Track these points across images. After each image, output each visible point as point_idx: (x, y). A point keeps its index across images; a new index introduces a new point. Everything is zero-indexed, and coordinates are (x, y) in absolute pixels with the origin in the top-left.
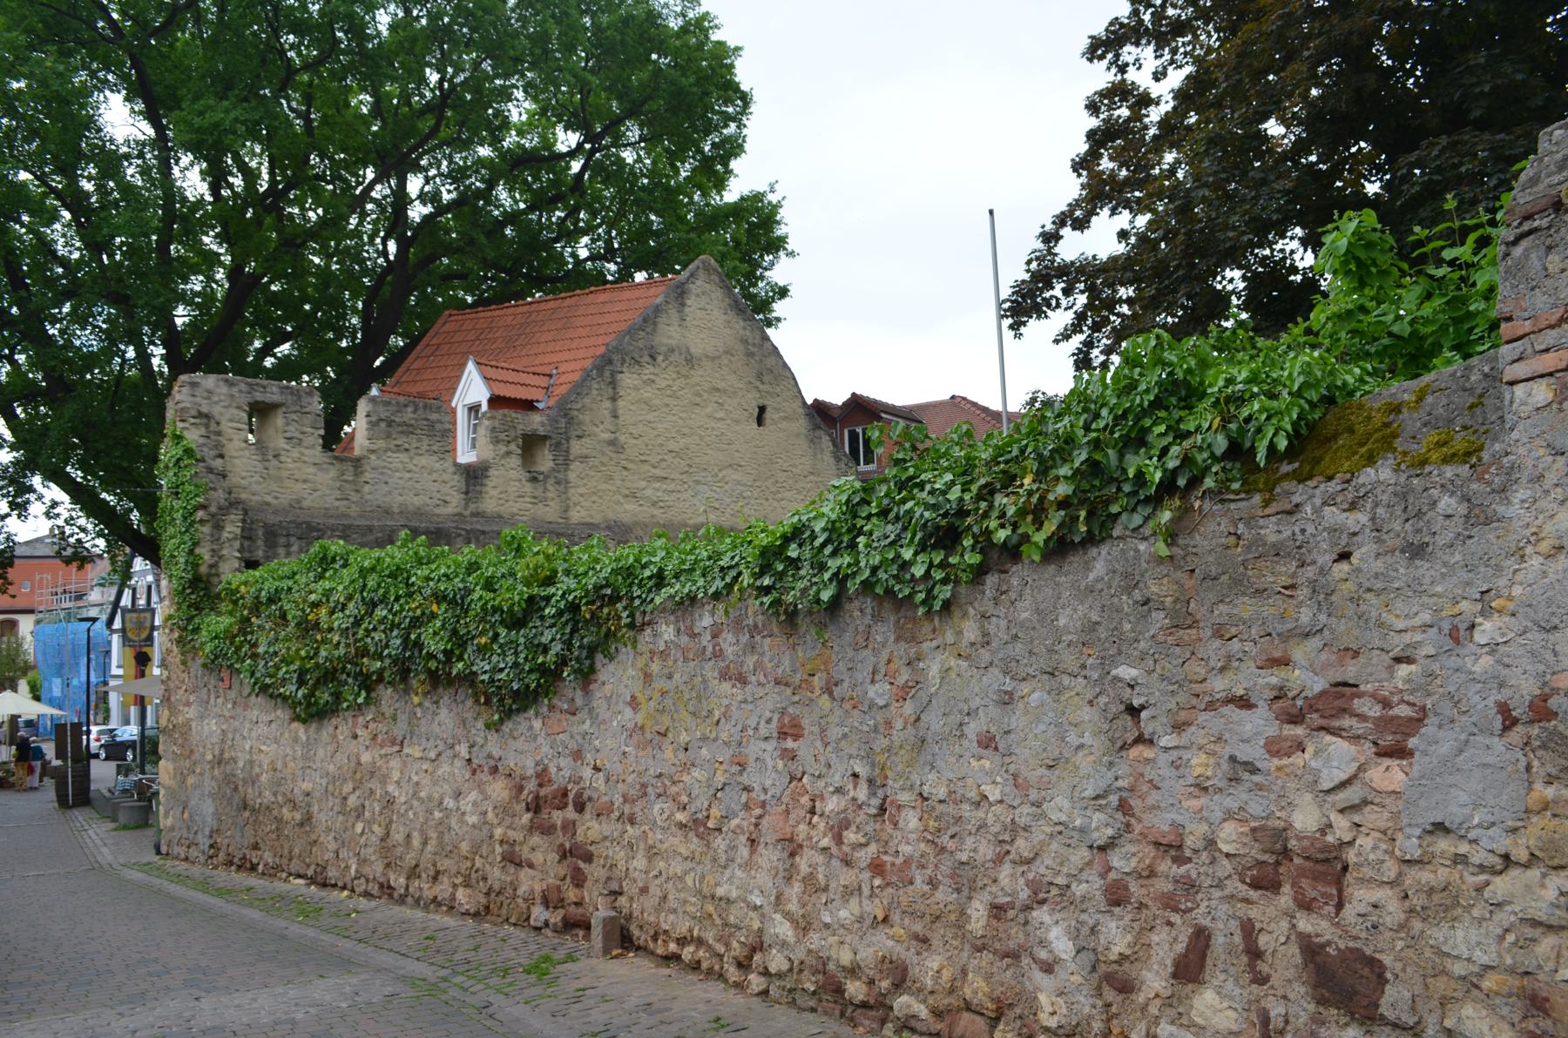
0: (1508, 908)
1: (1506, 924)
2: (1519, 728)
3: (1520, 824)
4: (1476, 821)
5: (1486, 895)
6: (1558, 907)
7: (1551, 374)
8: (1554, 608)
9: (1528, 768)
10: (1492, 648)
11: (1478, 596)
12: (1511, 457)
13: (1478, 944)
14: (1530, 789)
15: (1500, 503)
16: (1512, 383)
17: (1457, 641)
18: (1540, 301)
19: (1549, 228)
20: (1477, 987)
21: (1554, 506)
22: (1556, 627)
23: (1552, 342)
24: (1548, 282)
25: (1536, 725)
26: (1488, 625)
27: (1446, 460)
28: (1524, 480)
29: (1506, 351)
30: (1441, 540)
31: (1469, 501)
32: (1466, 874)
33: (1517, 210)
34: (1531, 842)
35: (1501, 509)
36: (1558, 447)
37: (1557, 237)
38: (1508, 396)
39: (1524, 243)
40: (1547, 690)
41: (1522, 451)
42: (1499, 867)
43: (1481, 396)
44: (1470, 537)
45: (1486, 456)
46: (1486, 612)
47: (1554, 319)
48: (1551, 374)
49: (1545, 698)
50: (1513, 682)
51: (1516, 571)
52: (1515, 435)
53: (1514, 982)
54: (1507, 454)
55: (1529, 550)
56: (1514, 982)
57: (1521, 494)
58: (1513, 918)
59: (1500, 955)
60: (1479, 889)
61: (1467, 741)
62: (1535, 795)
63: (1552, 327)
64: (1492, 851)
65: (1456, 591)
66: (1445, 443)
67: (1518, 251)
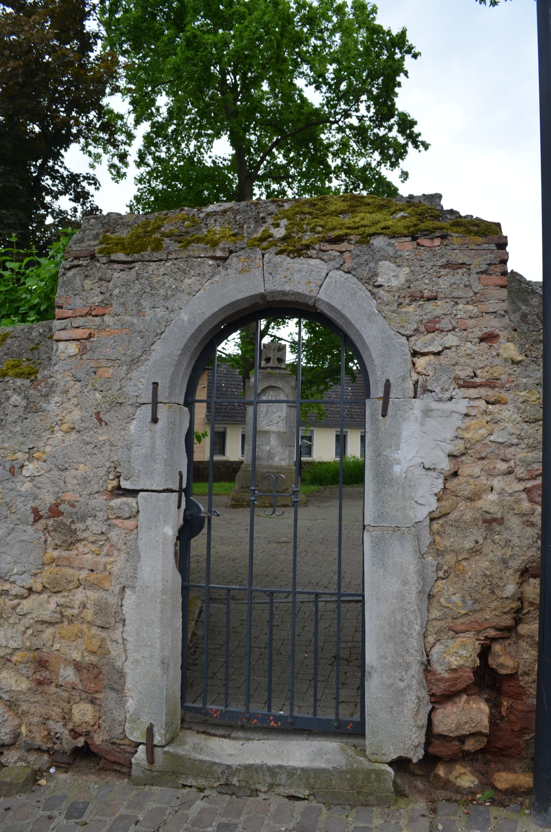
0: (29, 616)
1: (27, 625)
2: (42, 521)
3: (39, 571)
4: (15, 571)
5: (18, 611)
6: (55, 612)
7: (78, 340)
8: (66, 459)
9: (46, 541)
10: (32, 478)
11: (27, 450)
12: (53, 379)
13: (12, 637)
14: (45, 553)
15: (44, 402)
16: (58, 341)
17: (13, 474)
18: (78, 302)
19: (86, 266)
20: (9, 661)
21: (72, 407)
22: (66, 469)
23: (81, 324)
24: (84, 293)
25: (52, 519)
26: (31, 466)
27: (18, 376)
28: (58, 392)
29: (57, 324)
30: (10, 419)
31: (28, 399)
32: (7, 600)
33: (72, 253)
34: (44, 580)
35: (44, 406)
36: (78, 377)
37: (91, 272)
38: (55, 347)
39: (74, 271)
40: (59, 501)
41: (59, 376)
42: (26, 595)
43: (38, 344)
44: (26, 418)
45: (39, 376)
46: (31, 459)
47: (84, 312)
48: (78, 340)
49: (57, 505)
50: (42, 497)
51: (48, 439)
52: (56, 368)
53: (30, 655)
54: (51, 377)
55: (57, 428)
56: (30, 655)
57: (56, 399)
58: (31, 621)
59: (23, 642)
60: (14, 608)
61: (13, 528)
62: (48, 556)
63: (82, 316)
64: (23, 587)
65: (16, 447)
66: (17, 366)
67: (70, 274)
